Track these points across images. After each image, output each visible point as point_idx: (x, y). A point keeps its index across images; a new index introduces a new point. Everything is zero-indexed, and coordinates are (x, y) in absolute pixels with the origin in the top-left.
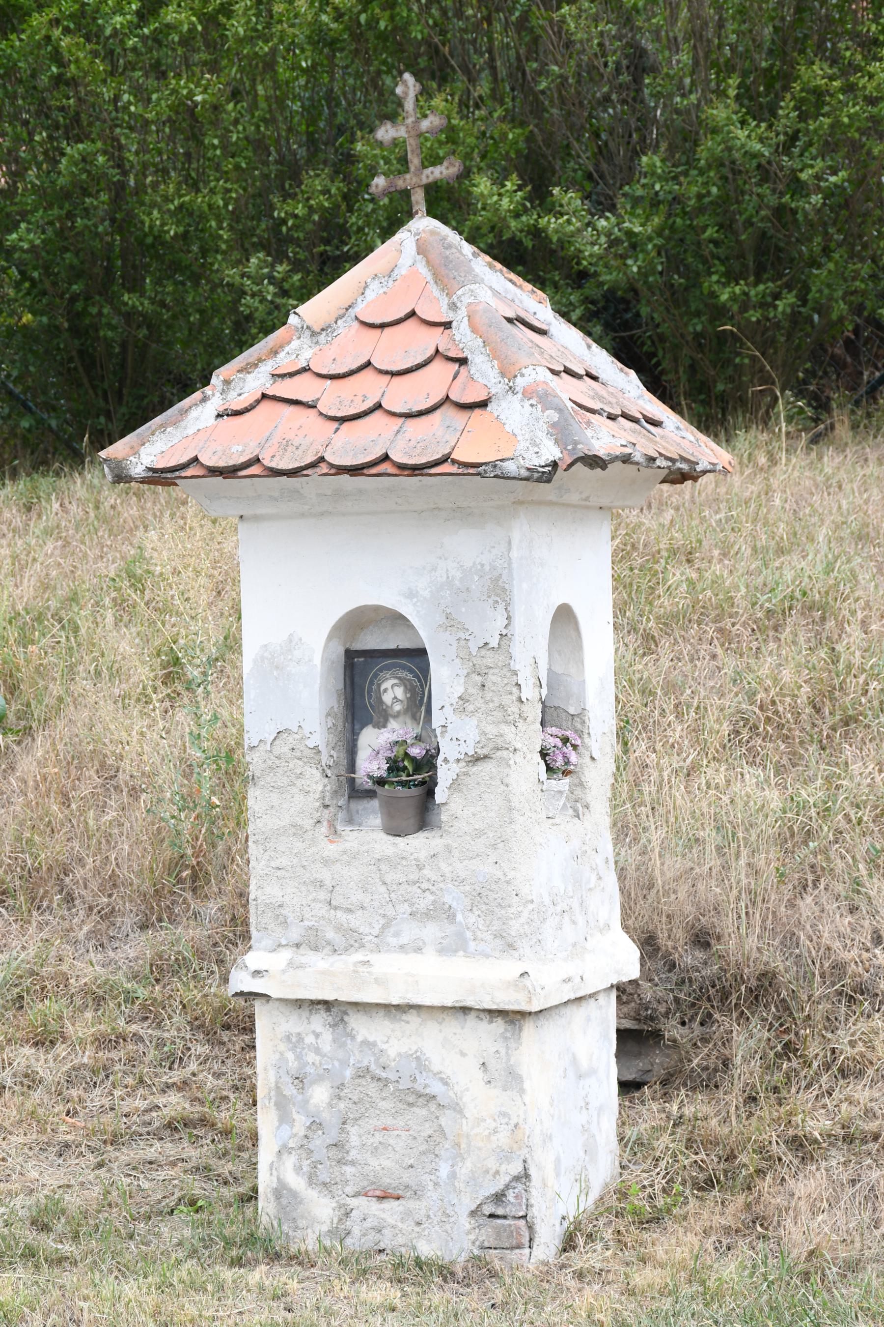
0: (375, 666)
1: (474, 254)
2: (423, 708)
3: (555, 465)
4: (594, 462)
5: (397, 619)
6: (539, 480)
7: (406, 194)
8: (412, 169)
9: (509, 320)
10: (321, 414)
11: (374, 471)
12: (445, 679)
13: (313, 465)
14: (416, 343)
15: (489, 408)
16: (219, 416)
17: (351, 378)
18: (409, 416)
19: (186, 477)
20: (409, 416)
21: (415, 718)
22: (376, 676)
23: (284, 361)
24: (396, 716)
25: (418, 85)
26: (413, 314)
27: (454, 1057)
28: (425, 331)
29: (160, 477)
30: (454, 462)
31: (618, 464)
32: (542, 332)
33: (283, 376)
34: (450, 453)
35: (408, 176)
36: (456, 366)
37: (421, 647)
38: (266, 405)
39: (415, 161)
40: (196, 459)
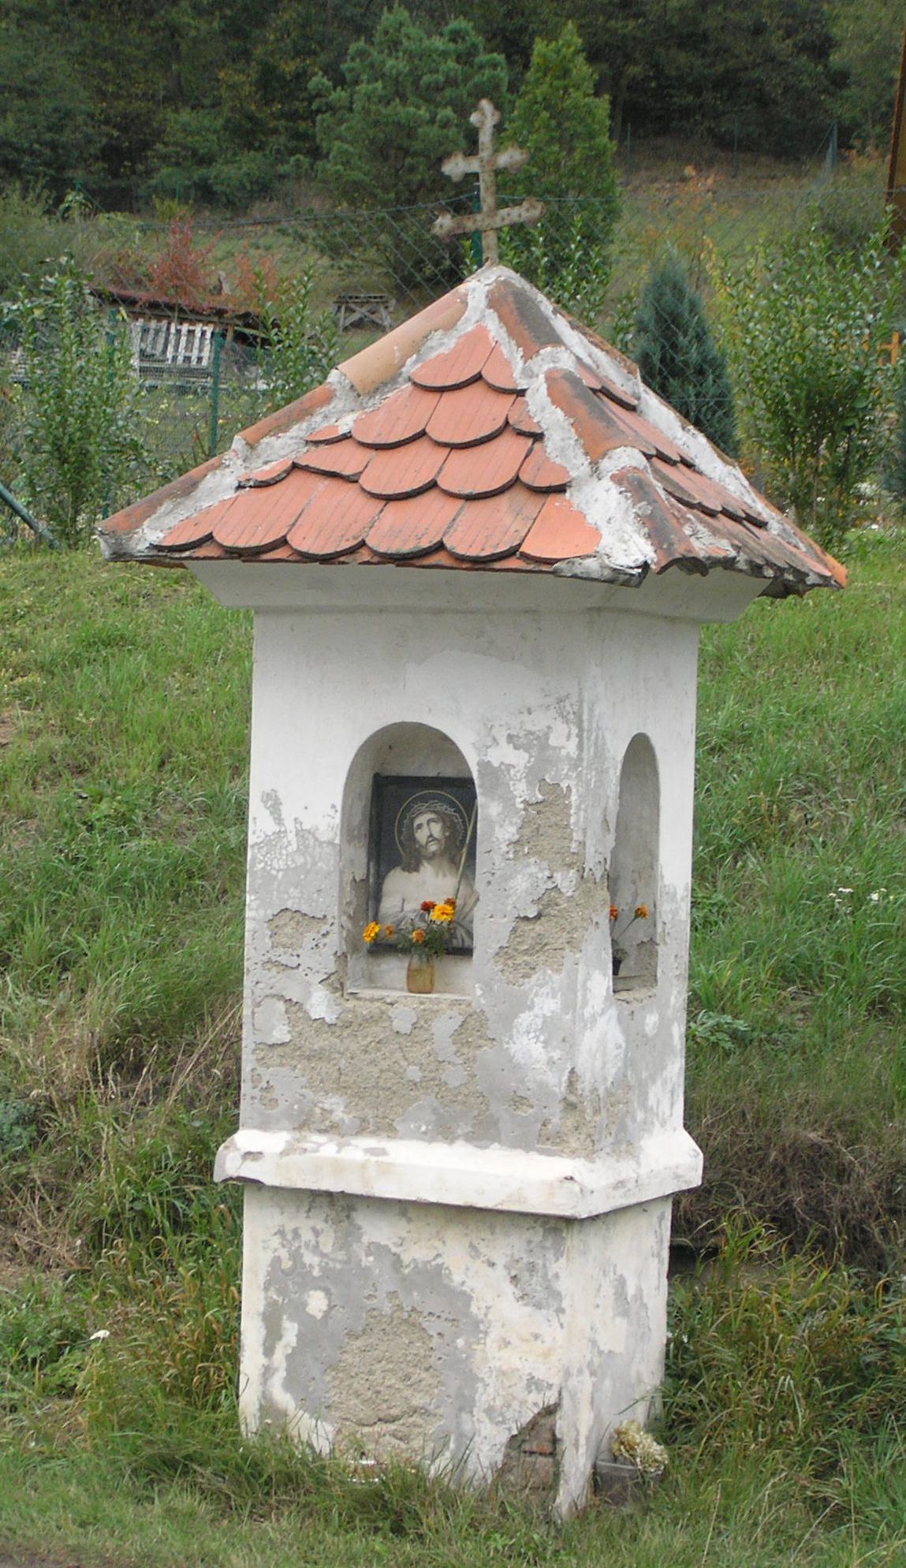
0: (408, 797)
1: (555, 312)
2: (465, 850)
3: (645, 566)
4: (694, 565)
5: (443, 744)
6: (626, 584)
7: (476, 235)
8: (485, 208)
9: (594, 391)
10: (364, 490)
11: (497, 565)
12: (497, 823)
13: (351, 551)
14: (478, 413)
15: (567, 494)
16: (240, 487)
17: (402, 450)
18: (471, 498)
19: (197, 558)
20: (471, 498)
21: (454, 862)
22: (409, 807)
23: (320, 423)
24: (431, 858)
25: (497, 114)
26: (478, 378)
27: (479, 1273)
28: (492, 397)
29: (164, 556)
30: (525, 557)
31: (719, 569)
32: (632, 409)
33: (317, 443)
34: (519, 545)
35: (479, 217)
36: (530, 441)
37: (466, 775)
38: (297, 478)
39: (488, 200)
40: (209, 537)
